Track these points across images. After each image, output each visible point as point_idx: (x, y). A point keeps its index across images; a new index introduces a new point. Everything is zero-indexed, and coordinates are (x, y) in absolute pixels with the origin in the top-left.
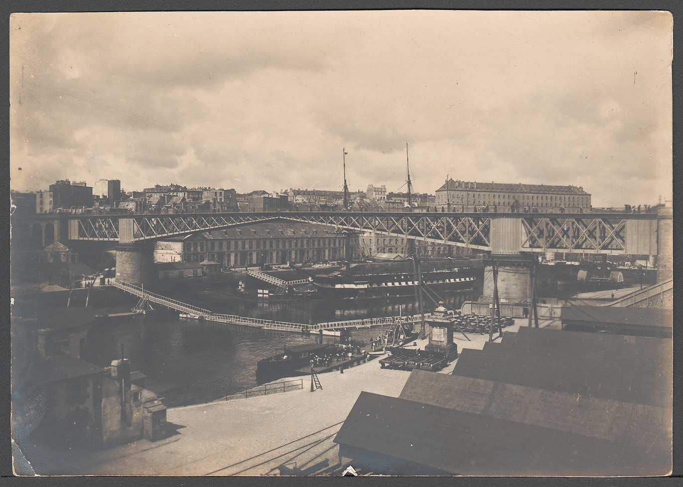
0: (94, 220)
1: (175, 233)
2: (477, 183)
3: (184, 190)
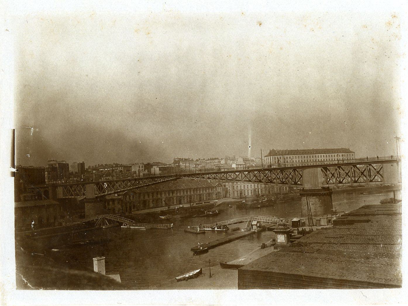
0: (71, 187)
1: (118, 191)
2: (288, 151)
3: (121, 166)
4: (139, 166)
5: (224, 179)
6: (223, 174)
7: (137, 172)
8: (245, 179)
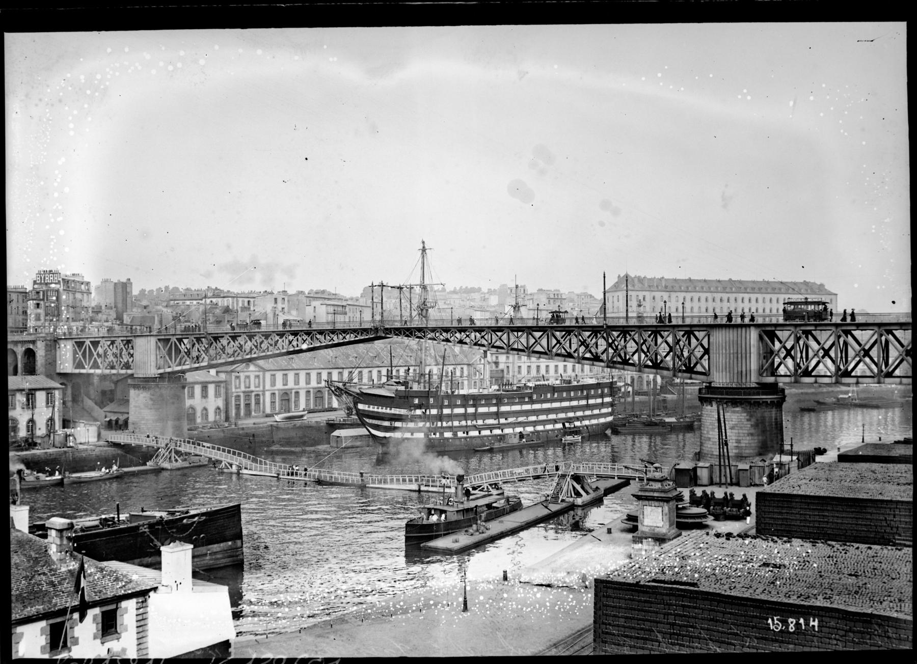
4: (276, 299)
5: (502, 348)
6: (499, 334)
7: (270, 316)
8: (558, 349)
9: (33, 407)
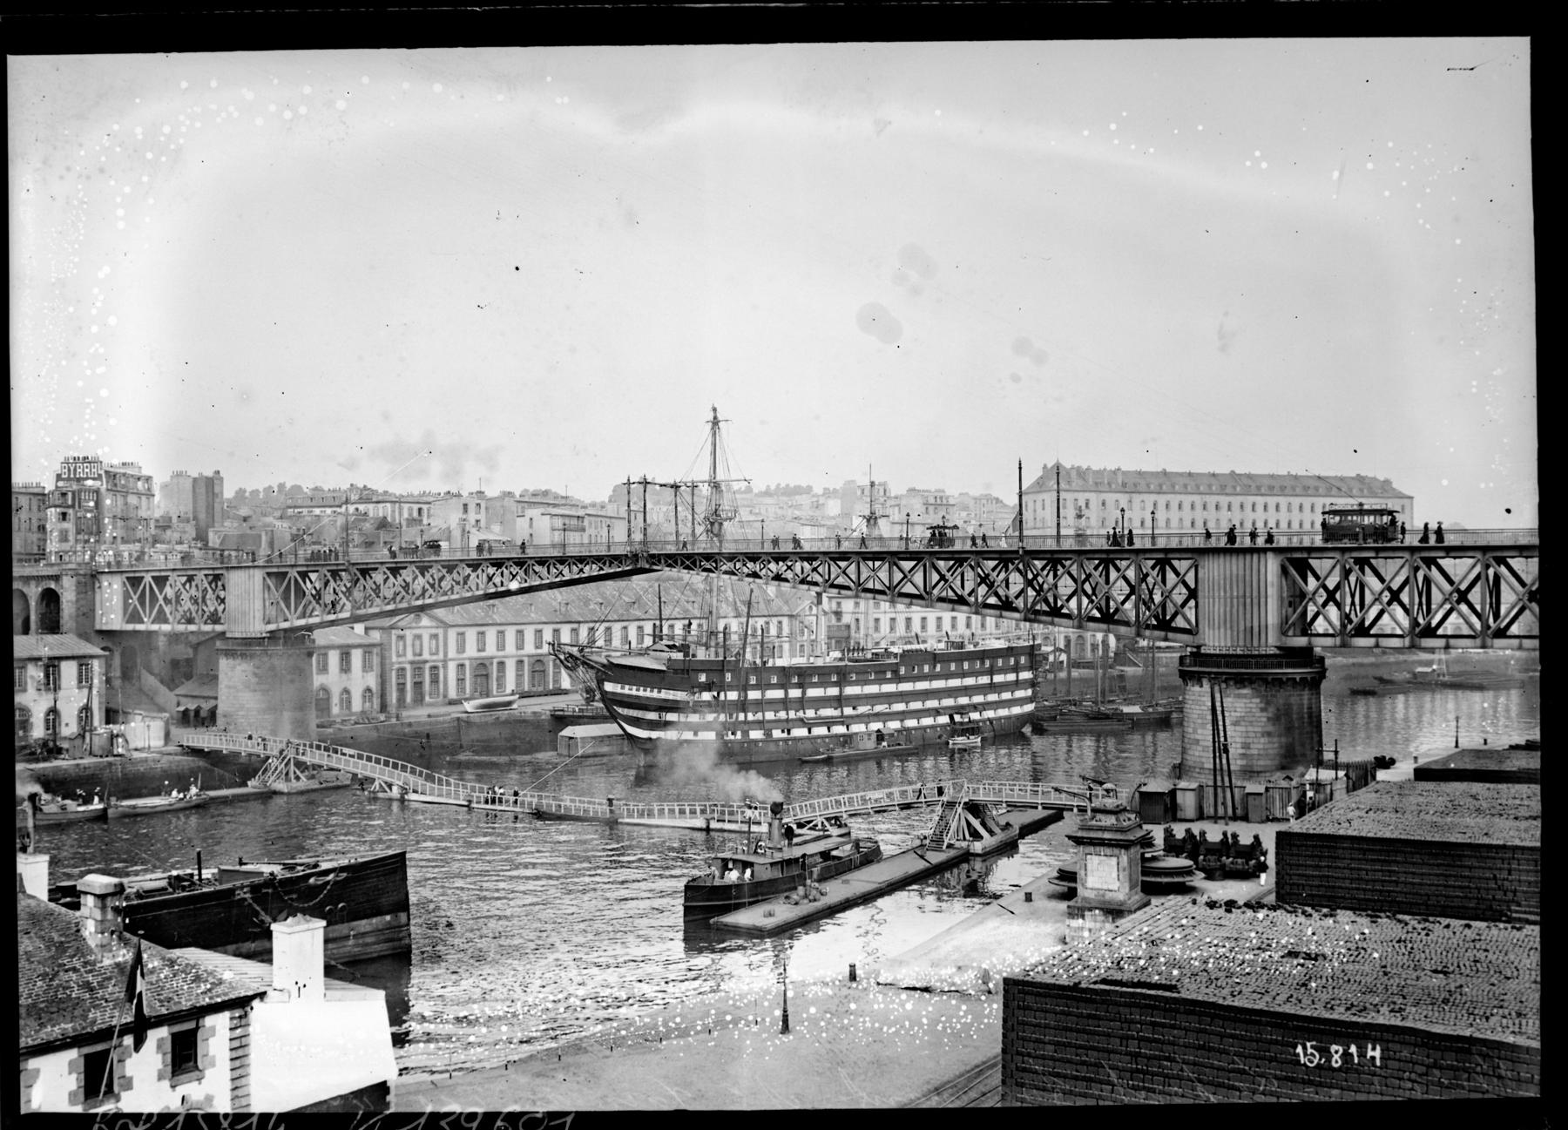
4: (465, 506)
6: (843, 564)
7: (457, 534)
9: (56, 689)
